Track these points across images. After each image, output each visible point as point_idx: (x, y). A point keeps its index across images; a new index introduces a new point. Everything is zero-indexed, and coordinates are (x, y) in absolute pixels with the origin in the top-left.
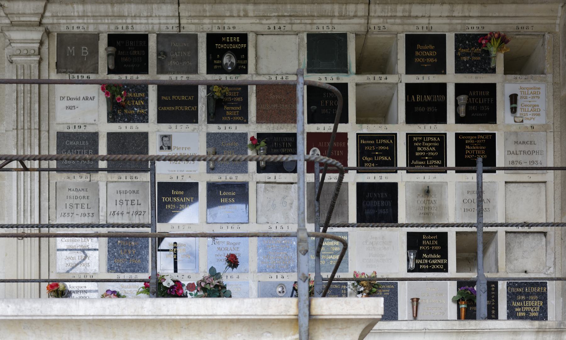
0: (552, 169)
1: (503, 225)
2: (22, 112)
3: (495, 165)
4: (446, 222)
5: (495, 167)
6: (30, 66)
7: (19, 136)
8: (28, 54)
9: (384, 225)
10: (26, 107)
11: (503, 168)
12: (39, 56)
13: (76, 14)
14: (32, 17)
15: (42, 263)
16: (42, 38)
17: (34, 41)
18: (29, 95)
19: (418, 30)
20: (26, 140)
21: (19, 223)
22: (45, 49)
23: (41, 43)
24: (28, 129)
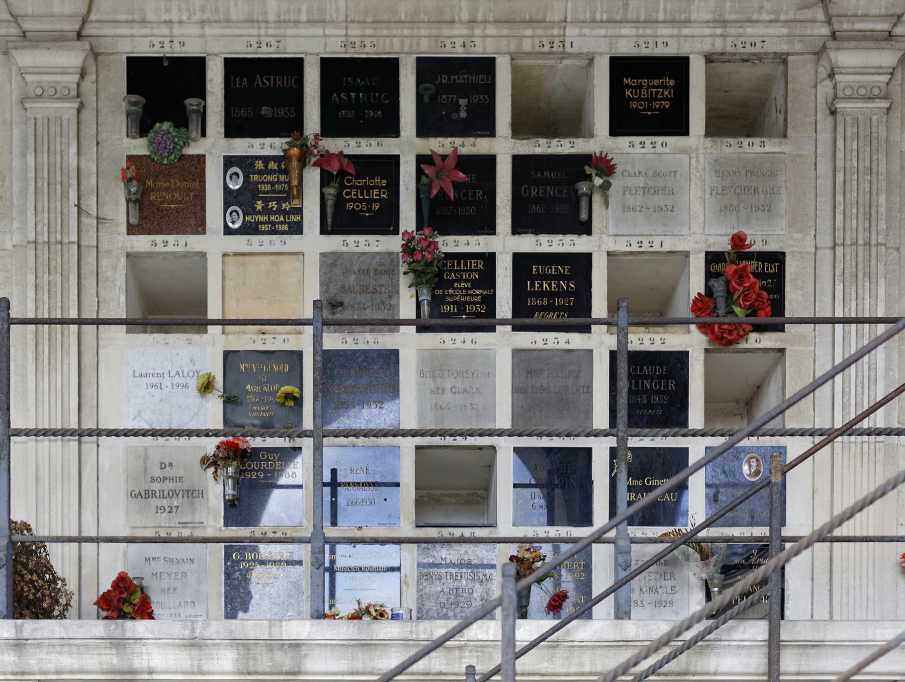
0: (74, 321)
1: (444, 433)
2: (855, 211)
3: (590, 316)
4: (490, 426)
5: (782, 318)
6: (871, 119)
7: (848, 257)
8: (57, 96)
9: (266, 432)
10: (861, 202)
11: (57, 321)
12: (79, 100)
13: (661, 17)
14: (879, 21)
15: (83, 504)
16: (84, 62)
17: (882, 71)
18: (869, 177)
19: (454, 50)
20: (860, 267)
21: (66, 427)
22: (88, 85)
23: (83, 74)
24: (865, 244)
